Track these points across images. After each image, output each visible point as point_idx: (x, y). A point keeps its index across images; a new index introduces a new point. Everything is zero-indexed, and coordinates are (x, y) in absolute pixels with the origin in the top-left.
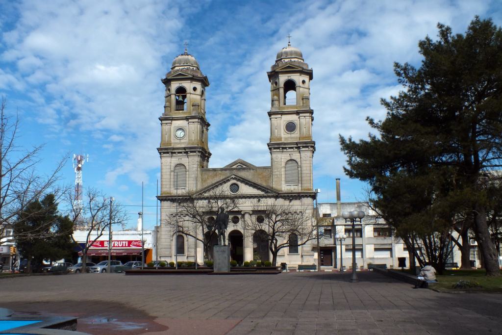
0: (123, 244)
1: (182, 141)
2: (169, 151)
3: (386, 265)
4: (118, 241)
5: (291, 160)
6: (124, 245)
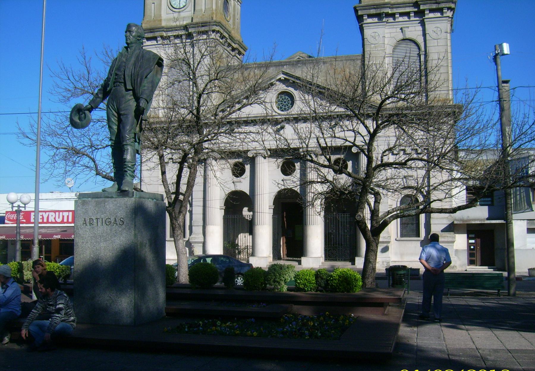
0: (63, 217)
1: (183, 14)
2: (157, 34)
3: (419, 269)
4: (55, 212)
5: (403, 40)
6: (65, 220)
